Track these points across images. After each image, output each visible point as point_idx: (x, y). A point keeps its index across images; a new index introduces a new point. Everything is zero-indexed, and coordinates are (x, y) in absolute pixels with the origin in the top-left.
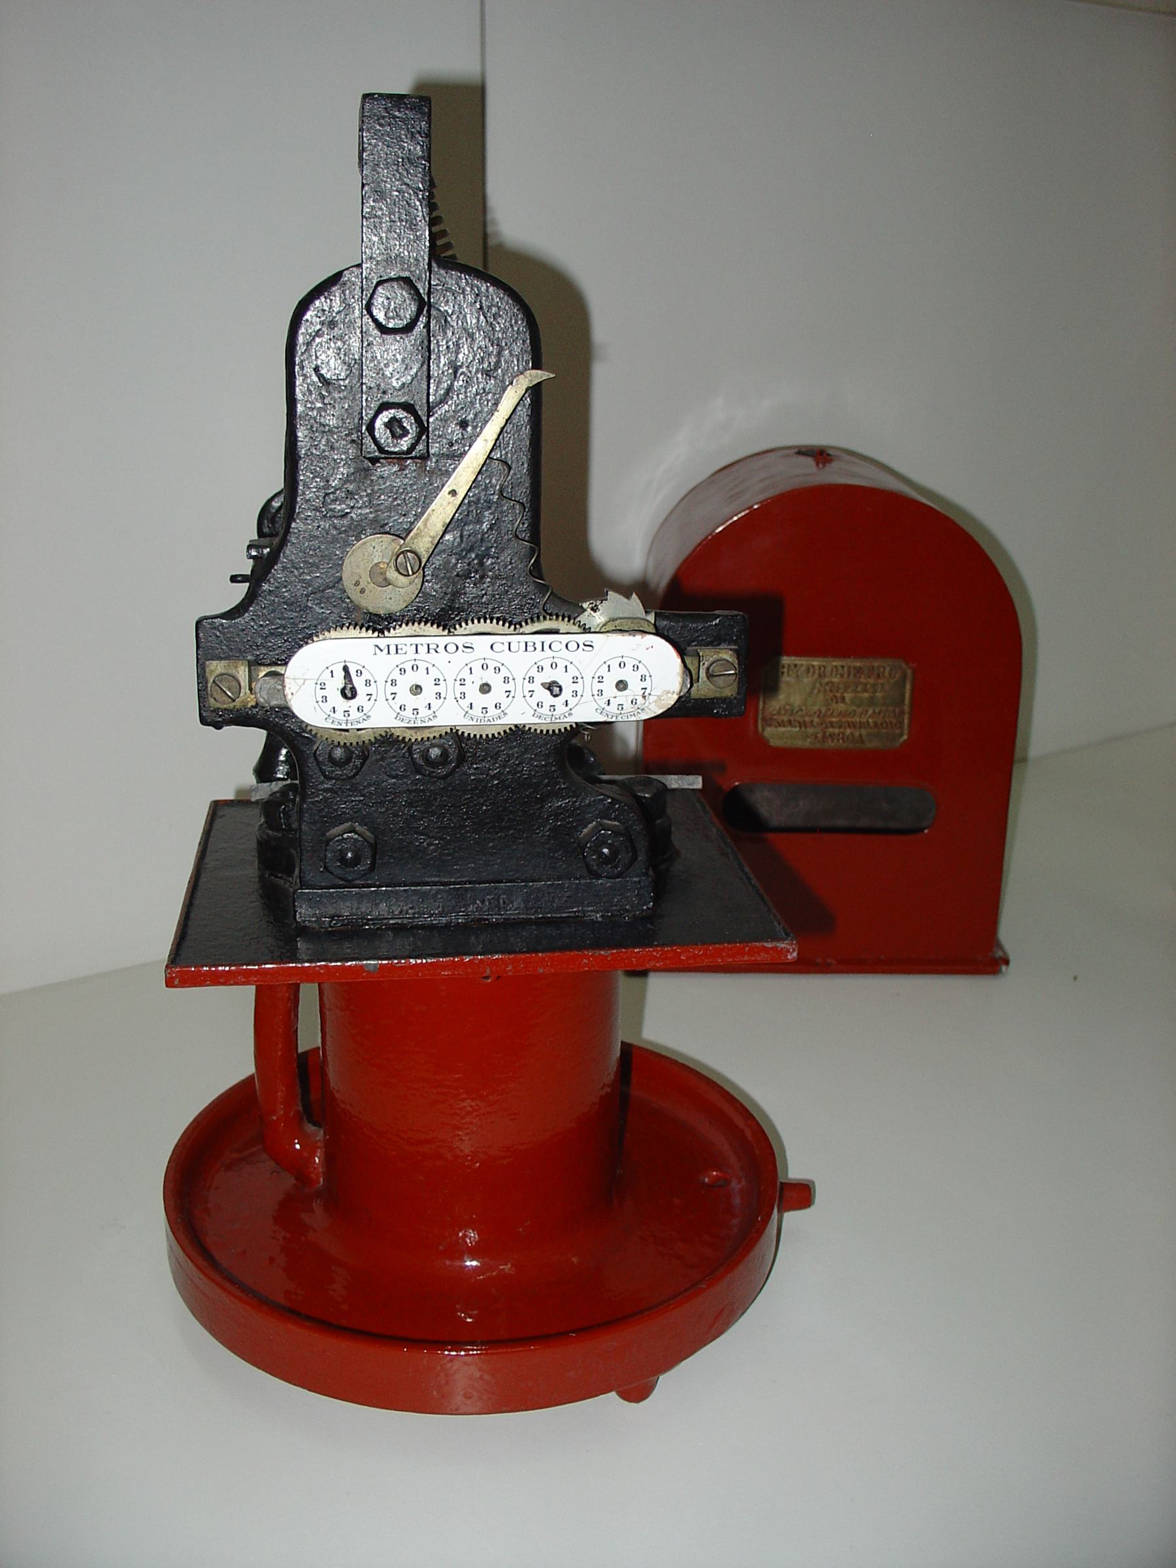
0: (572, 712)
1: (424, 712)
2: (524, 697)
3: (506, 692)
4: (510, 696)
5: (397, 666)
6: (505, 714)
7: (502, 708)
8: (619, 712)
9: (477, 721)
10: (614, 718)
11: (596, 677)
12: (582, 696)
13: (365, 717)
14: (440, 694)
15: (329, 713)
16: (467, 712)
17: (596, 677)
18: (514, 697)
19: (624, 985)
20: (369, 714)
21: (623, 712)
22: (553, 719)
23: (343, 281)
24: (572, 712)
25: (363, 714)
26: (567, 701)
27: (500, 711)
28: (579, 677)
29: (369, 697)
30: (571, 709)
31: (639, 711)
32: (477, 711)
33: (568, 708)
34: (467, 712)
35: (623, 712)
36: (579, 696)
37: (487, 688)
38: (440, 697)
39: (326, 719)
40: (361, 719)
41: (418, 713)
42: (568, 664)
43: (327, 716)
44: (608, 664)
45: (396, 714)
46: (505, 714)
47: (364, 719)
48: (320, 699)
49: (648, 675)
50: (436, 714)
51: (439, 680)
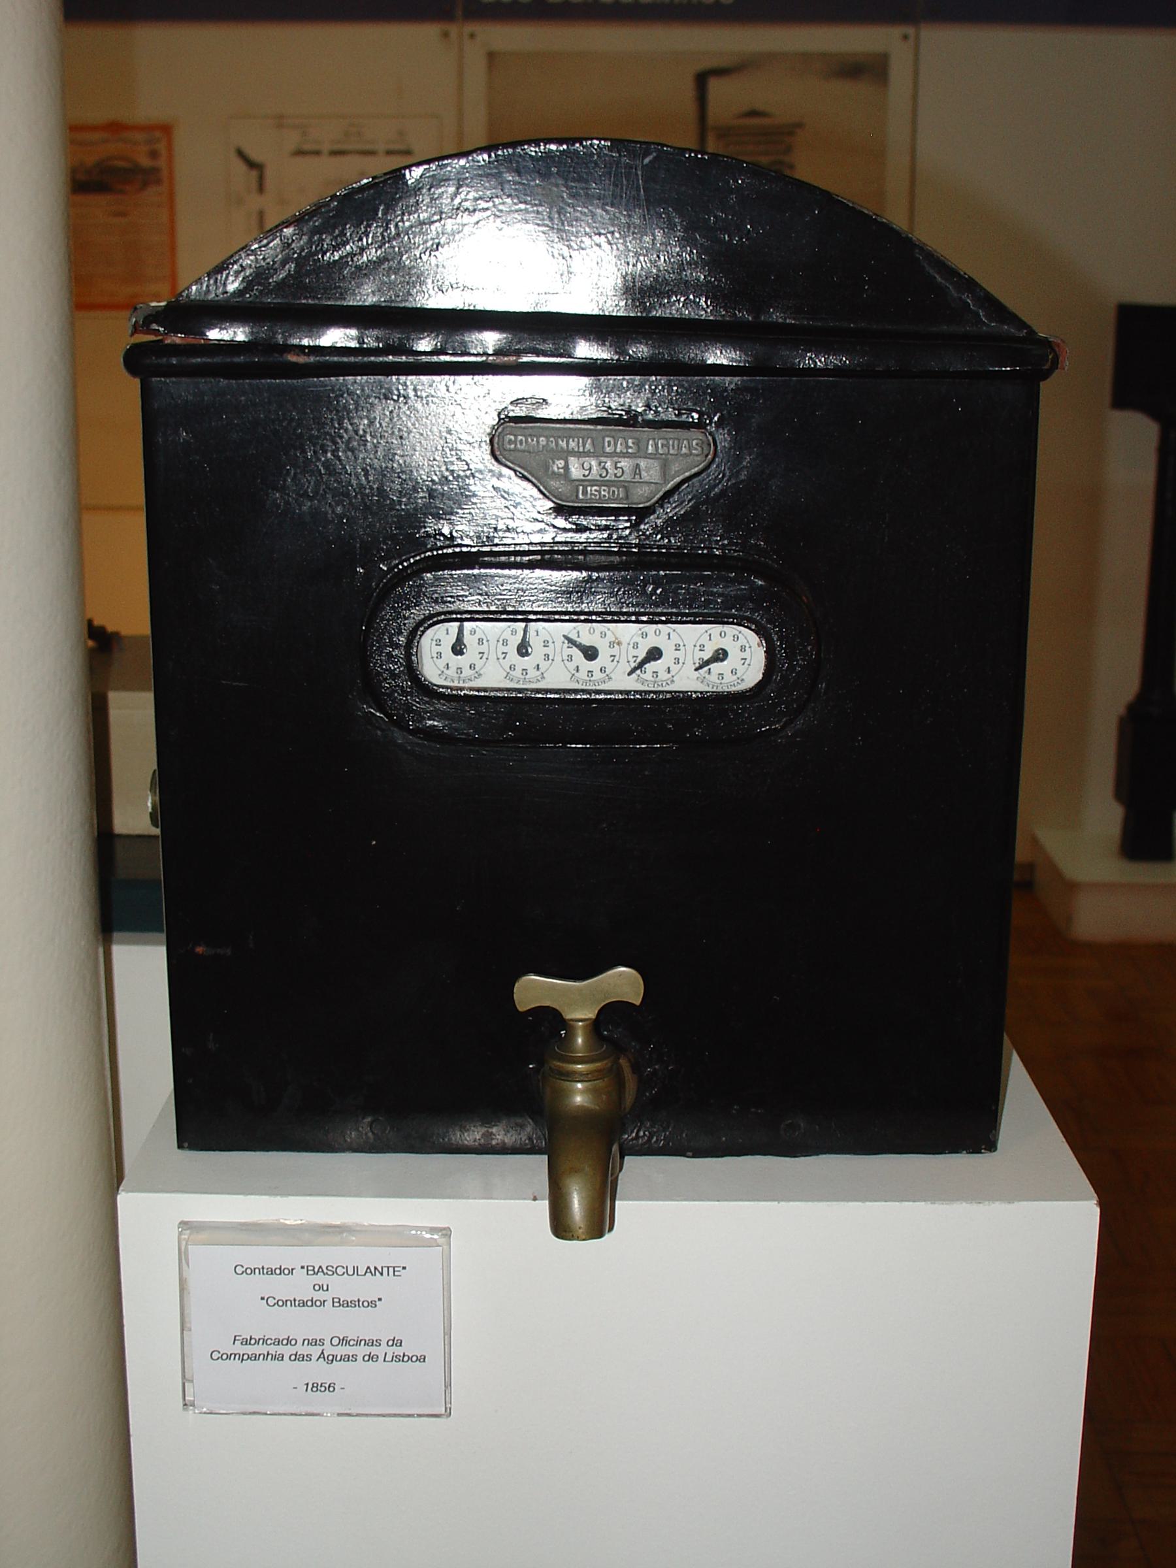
0: (674, 679)
1: (533, 673)
2: (628, 662)
3: (742, 659)
4: (746, 664)
5: (706, 632)
6: (480, 675)
7: (477, 669)
8: (719, 682)
9: (713, 688)
10: (715, 688)
11: (698, 645)
12: (683, 663)
13: (476, 675)
14: (548, 655)
15: (443, 669)
16: (573, 675)
17: (698, 645)
18: (749, 665)
19: (163, 936)
20: (481, 672)
21: (723, 681)
22: (656, 685)
23: (345, 384)
24: (674, 679)
25: (474, 671)
26: (669, 668)
27: (605, 675)
28: (551, 641)
29: (481, 655)
30: (673, 677)
31: (739, 681)
32: (582, 675)
33: (670, 675)
34: (508, 673)
35: (723, 681)
36: (681, 664)
37: (658, 654)
38: (548, 659)
39: (440, 675)
40: (736, 683)
41: (527, 674)
42: (671, 631)
43: (440, 673)
44: (709, 632)
45: (505, 674)
46: (610, 678)
47: (475, 677)
48: (565, 658)
49: (747, 646)
50: (545, 675)
51: (548, 642)
